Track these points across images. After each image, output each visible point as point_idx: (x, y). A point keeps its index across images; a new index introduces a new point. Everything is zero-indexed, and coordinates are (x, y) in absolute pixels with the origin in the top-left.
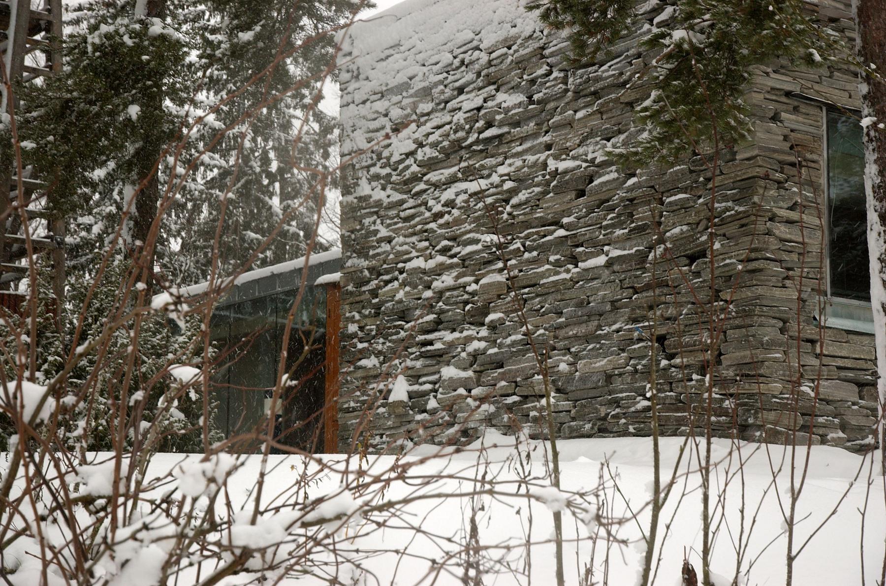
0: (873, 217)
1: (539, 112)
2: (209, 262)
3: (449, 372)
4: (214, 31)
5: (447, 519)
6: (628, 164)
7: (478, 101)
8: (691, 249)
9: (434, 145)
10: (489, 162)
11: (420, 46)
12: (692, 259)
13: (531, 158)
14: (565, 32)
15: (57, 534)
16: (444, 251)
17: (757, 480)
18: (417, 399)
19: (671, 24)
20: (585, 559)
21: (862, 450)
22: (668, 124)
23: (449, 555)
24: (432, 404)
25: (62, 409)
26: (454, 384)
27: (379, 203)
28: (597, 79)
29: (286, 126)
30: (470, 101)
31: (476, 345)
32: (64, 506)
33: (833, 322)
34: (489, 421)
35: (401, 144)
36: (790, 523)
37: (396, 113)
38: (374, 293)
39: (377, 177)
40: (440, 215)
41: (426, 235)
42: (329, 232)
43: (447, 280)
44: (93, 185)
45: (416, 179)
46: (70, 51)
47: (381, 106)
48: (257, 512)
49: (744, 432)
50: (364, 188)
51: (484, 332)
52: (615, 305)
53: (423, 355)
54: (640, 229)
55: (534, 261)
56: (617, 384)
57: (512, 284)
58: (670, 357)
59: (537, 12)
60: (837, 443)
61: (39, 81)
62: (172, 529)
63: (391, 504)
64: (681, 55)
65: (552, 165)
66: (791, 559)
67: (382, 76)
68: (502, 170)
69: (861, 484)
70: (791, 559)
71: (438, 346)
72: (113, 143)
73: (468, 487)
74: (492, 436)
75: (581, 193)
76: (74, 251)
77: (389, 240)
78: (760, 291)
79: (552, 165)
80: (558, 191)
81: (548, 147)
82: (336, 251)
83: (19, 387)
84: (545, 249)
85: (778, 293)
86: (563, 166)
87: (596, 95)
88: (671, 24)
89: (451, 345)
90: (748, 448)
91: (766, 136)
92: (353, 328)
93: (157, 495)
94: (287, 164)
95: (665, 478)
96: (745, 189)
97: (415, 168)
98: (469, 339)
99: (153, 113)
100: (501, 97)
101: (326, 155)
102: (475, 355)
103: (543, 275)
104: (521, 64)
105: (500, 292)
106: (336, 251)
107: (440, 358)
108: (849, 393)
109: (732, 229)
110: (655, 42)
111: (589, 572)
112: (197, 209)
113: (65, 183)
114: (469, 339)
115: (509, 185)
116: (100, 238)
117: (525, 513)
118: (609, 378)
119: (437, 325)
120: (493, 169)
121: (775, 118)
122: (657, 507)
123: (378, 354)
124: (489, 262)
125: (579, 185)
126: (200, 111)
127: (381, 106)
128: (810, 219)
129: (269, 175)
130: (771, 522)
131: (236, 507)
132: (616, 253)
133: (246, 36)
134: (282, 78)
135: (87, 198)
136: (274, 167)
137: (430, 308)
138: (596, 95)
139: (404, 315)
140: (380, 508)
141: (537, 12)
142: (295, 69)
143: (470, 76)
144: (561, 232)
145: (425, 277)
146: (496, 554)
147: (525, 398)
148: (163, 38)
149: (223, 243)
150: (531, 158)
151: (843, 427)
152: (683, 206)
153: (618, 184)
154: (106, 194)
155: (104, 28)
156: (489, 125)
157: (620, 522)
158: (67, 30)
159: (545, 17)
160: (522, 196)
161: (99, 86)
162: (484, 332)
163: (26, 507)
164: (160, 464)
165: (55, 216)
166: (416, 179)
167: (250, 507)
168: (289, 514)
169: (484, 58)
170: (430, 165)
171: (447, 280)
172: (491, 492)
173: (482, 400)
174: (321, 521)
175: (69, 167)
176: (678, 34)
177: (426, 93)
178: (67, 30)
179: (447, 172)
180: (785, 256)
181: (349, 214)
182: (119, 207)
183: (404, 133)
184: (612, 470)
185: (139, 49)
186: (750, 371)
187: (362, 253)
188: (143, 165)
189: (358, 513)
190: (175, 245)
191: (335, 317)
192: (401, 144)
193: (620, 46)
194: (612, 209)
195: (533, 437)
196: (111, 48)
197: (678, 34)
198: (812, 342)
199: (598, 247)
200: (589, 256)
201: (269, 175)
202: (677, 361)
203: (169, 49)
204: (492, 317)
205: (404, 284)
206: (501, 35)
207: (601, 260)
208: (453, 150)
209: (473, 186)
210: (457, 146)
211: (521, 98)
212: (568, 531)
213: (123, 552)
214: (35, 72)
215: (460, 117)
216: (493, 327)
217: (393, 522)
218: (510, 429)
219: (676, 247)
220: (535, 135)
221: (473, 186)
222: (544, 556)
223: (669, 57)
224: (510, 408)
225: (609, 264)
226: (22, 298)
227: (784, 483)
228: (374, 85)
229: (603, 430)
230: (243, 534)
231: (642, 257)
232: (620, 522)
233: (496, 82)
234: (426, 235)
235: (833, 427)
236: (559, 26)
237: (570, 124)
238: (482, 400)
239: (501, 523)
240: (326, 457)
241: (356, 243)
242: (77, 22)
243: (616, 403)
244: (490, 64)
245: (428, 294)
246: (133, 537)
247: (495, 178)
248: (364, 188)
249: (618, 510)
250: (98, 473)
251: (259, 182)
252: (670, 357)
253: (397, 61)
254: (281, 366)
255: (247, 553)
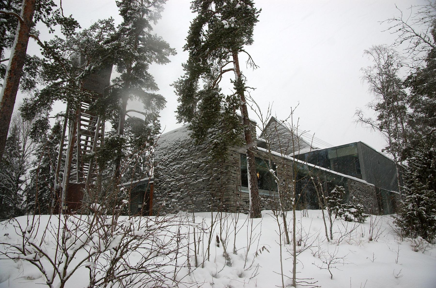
0: (248, 173)
1: (191, 153)
2: (129, 179)
3: (173, 200)
4: (132, 137)
5: (174, 229)
6: (206, 163)
7: (180, 151)
8: (217, 178)
9: (171, 158)
10: (181, 161)
11: (169, 141)
12: (218, 179)
13: (189, 161)
14: (195, 139)
15: (101, 232)
16: (173, 178)
17: (230, 220)
18: (167, 205)
19: (214, 138)
20: (199, 235)
21: (247, 213)
22: (214, 156)
23: (175, 236)
24: (170, 206)
25: (103, 208)
26: (174, 202)
27: (161, 169)
28: (201, 147)
29: (145, 154)
30: (178, 151)
31: (178, 195)
32: (103, 226)
33: (242, 191)
34: (181, 209)
35: (166, 157)
36: (235, 228)
37: (164, 152)
38: (160, 185)
39: (161, 164)
40: (172, 171)
41: (170, 175)
42: (151, 173)
43: (173, 183)
44: (108, 164)
45: (168, 164)
46: (105, 140)
47: (162, 151)
48: (139, 228)
49: (227, 211)
50: (158, 166)
51: (180, 193)
52: (204, 188)
53: (168, 197)
54: (208, 174)
55: (189, 180)
56: (204, 202)
57: (186, 184)
58: (214, 197)
59: (190, 136)
60: (242, 212)
61: (99, 146)
62: (124, 232)
63: (164, 227)
64: (216, 144)
65: (193, 162)
66: (235, 234)
67: (162, 146)
68: (184, 163)
69: (247, 220)
70: (235, 234)
71: (171, 195)
72: (112, 157)
73: (178, 223)
74: (180, 212)
75: (198, 168)
76: (104, 176)
77: (162, 175)
78: (230, 186)
79: (193, 162)
80: (194, 167)
81: (192, 159)
82: (153, 177)
83: (96, 204)
84: (191, 177)
85: (233, 186)
86: (195, 163)
87: (201, 150)
88: (214, 138)
89: (174, 195)
90: (228, 214)
91: (230, 158)
92: (155, 192)
93: (120, 225)
94: (144, 161)
95: (214, 221)
96: (227, 168)
97: (168, 162)
98: (177, 194)
99: (120, 151)
100: (184, 150)
101: (152, 159)
102: (178, 197)
103: (191, 182)
104: (187, 144)
105: (182, 185)
106: (153, 177)
107: (172, 197)
108: (245, 203)
109: (225, 174)
110: (211, 142)
111: (200, 238)
112: (127, 169)
113: (104, 164)
114: (177, 194)
115: (185, 166)
116: (109, 174)
117: (188, 228)
118: (203, 201)
119: (171, 191)
120: (182, 163)
121: (232, 155)
122: (212, 226)
123: (160, 197)
124: (180, 180)
125: (197, 166)
126: (129, 151)
127: (162, 151)
128: (238, 173)
129: (141, 163)
130: (232, 228)
131: (135, 227)
132: (204, 178)
133: (138, 138)
134: (145, 146)
135: (107, 166)
136: (142, 161)
137: (170, 188)
138: (201, 150)
139: (165, 189)
140: (162, 227)
141: (190, 136)
142: (147, 144)
143: (178, 146)
144: (194, 175)
145: (169, 183)
146: (184, 236)
147: (187, 205)
148: (122, 138)
149: (131, 175)
150: (189, 161)
151: (243, 210)
152: (216, 170)
153: (205, 166)
154: (110, 166)
155: (112, 136)
156: (181, 155)
157: (206, 229)
158: (105, 137)
159: (191, 137)
160: (187, 168)
161: (110, 147)
162: (180, 193)
163: (96, 227)
164: (121, 218)
165: (102, 169)
166: (168, 164)
167: (138, 227)
168: (145, 229)
169: (181, 143)
170: (170, 162)
171: (173, 183)
172: (183, 224)
173: (179, 205)
174: (151, 230)
175: (104, 162)
176: (215, 141)
177: (170, 149)
178: (105, 137)
179: (174, 163)
180: (233, 179)
181: (155, 170)
182: (113, 168)
183: (166, 156)
184: (204, 219)
185: (118, 141)
186: (227, 200)
187: (158, 178)
188: (117, 162)
189: (5, 58)
190: (122, 176)
191: (152, 189)
192: (166, 157)
193: (204, 142)
194: (203, 171)
195: (189, 212)
196: (113, 140)
197: (215, 141)
198: (239, 195)
199: (201, 177)
200: (199, 179)
201: (141, 163)
202: (215, 198)
203: (123, 140)
204: (181, 190)
205: (165, 184)
206: (184, 139)
207: (201, 180)
208: (175, 159)
209: (179, 166)
210: (176, 158)
211: (187, 150)
212: (196, 231)
213: (114, 237)
214: (99, 144)
215: (176, 153)
216: (182, 192)
217: (165, 230)
218: (184, 211)
219: (215, 177)
220: (190, 157)
221: (179, 166)
222: (192, 236)
223: (214, 144)
224: (185, 207)
225: (203, 181)
226: (94, 185)
227: (234, 221)
228: (160, 147)
229: (202, 211)
230: (136, 233)
231: (209, 179)
232: (206, 229)
233: (182, 147)
234: (170, 175)
235: (242, 210)
236: (194, 138)
237: (196, 155)
238: (179, 205)
239: (184, 230)
240: (151, 217)
241: (156, 176)
242: (107, 135)
243: (204, 206)
244: (182, 144)
245: (170, 185)
246: (116, 234)
247: (182, 165)
248: (158, 166)
249: (205, 228)
250: (109, 219)
251: (139, 164)
252: (214, 197)
253: (165, 143)
254: (144, 201)
255: (137, 236)
